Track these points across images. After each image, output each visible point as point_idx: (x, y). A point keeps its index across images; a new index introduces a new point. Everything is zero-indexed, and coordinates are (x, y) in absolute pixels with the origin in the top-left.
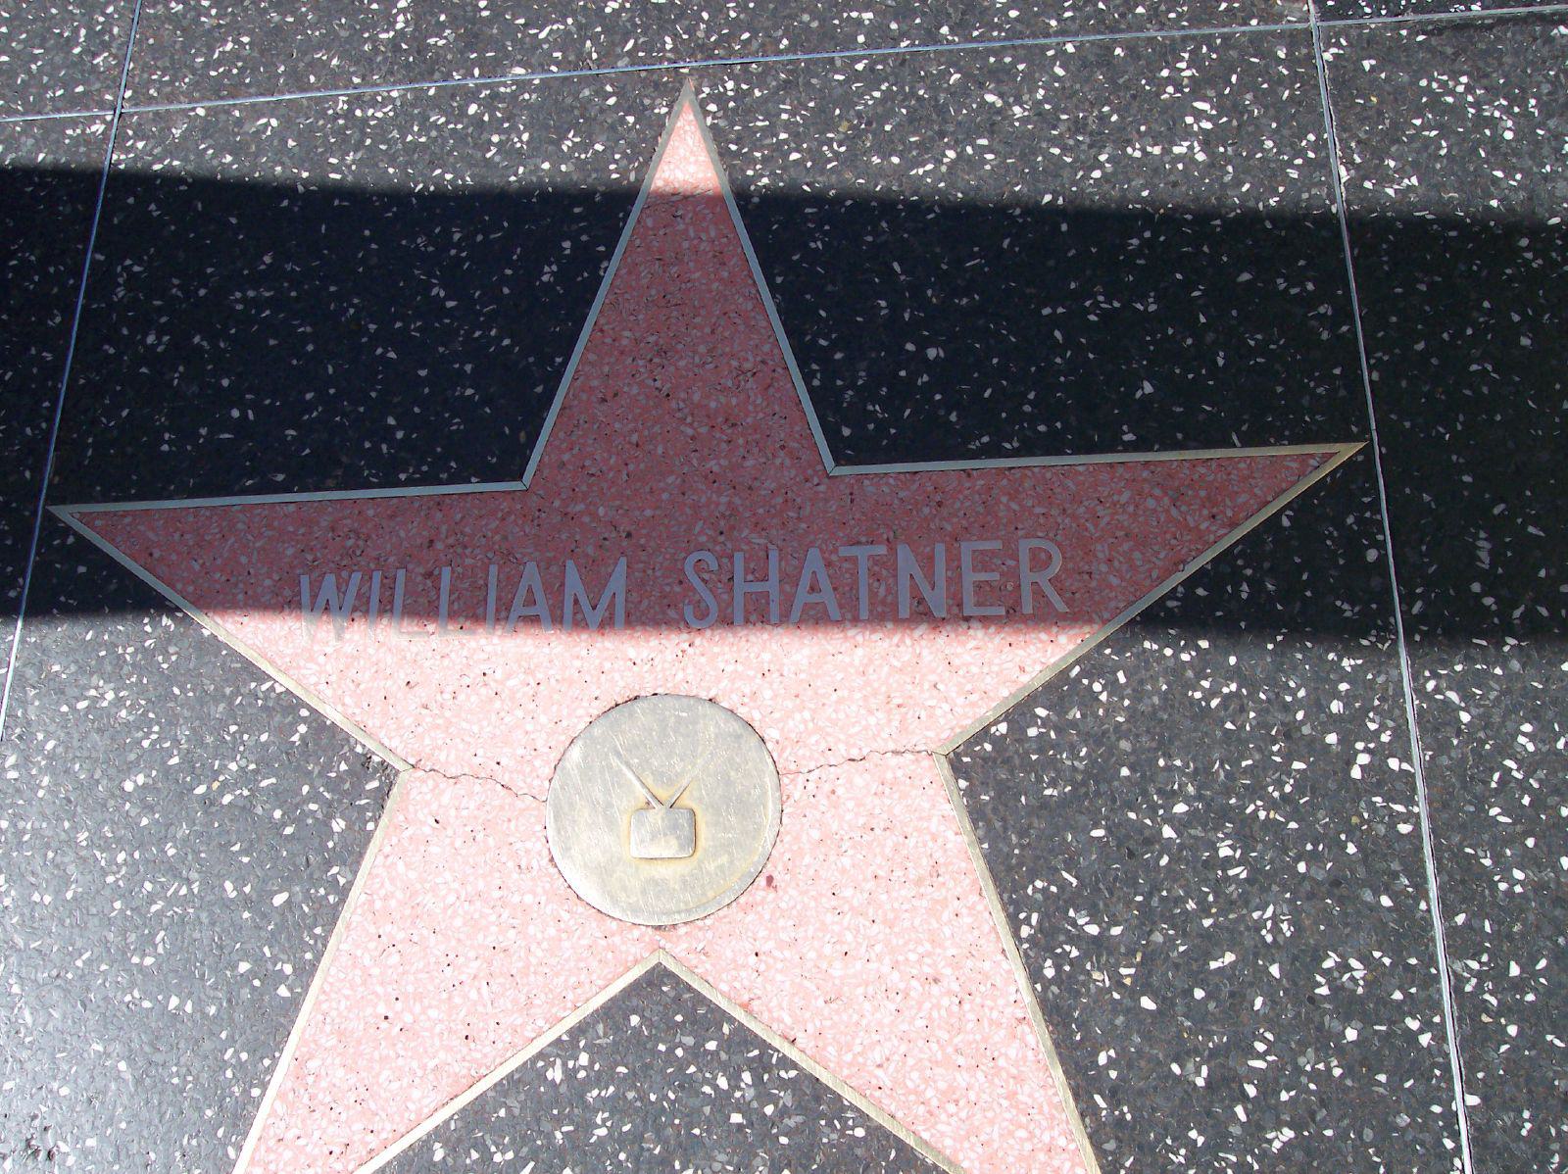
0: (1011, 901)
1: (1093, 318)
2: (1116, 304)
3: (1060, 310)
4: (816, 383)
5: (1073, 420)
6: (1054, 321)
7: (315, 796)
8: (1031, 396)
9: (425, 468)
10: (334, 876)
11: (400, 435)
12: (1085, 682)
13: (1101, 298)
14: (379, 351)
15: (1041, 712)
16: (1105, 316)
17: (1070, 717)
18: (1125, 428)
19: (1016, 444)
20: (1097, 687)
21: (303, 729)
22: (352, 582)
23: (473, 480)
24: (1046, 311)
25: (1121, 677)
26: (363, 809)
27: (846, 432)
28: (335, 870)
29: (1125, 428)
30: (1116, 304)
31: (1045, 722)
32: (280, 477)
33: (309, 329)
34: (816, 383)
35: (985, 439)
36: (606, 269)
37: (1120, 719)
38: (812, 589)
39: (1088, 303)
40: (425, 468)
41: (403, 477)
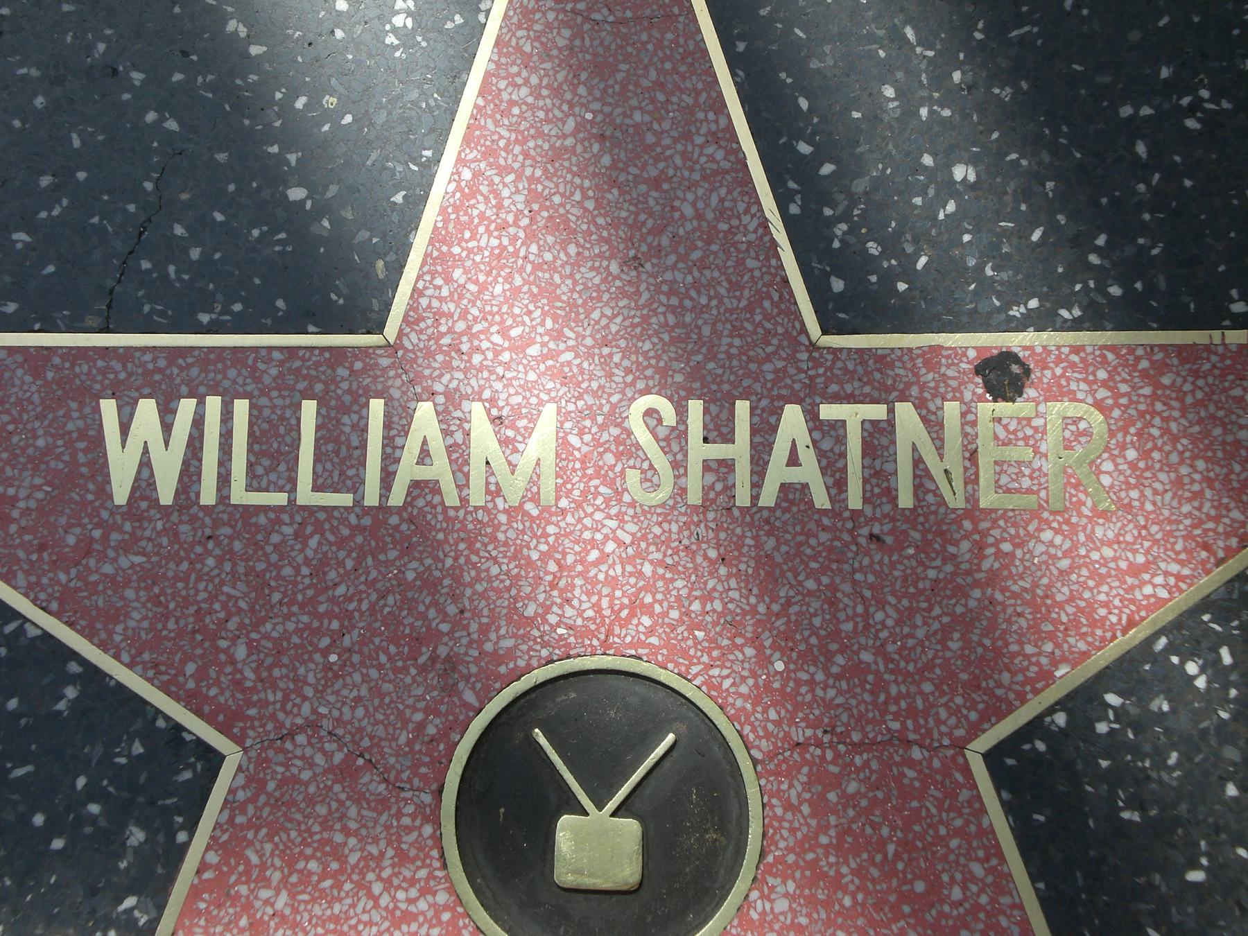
0: (498, 64)
1: (1191, 124)
2: (1225, 104)
3: (1146, 111)
4: (794, 209)
5: (1162, 283)
6: (1134, 128)
7: (93, 793)
8: (1101, 241)
9: (237, 307)
10: (129, 911)
11: (195, 253)
12: (1175, 660)
13: (1205, 94)
14: (151, 117)
15: (1113, 699)
16: (1213, 122)
17: (1154, 706)
18: (1234, 293)
19: (1077, 312)
20: (1192, 668)
21: (71, 692)
22: (455, 492)
23: (311, 328)
24: (1126, 111)
25: (1226, 657)
26: (168, 812)
27: (838, 285)
28: (130, 902)
29: (1234, 293)
30: (1225, 104)
31: (1120, 713)
32: (11, 307)
33: (35, 72)
34: (794, 209)
35: (1033, 303)
36: (488, 12)
37: (1224, 715)
38: (420, 462)
39: (1185, 101)
40: (237, 307)
41: (205, 318)
